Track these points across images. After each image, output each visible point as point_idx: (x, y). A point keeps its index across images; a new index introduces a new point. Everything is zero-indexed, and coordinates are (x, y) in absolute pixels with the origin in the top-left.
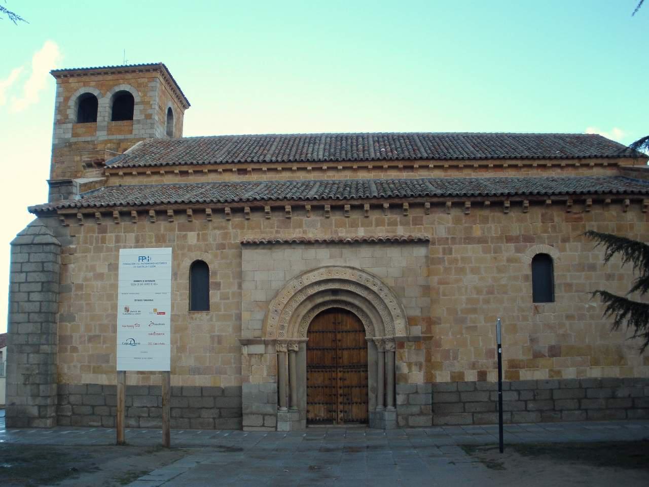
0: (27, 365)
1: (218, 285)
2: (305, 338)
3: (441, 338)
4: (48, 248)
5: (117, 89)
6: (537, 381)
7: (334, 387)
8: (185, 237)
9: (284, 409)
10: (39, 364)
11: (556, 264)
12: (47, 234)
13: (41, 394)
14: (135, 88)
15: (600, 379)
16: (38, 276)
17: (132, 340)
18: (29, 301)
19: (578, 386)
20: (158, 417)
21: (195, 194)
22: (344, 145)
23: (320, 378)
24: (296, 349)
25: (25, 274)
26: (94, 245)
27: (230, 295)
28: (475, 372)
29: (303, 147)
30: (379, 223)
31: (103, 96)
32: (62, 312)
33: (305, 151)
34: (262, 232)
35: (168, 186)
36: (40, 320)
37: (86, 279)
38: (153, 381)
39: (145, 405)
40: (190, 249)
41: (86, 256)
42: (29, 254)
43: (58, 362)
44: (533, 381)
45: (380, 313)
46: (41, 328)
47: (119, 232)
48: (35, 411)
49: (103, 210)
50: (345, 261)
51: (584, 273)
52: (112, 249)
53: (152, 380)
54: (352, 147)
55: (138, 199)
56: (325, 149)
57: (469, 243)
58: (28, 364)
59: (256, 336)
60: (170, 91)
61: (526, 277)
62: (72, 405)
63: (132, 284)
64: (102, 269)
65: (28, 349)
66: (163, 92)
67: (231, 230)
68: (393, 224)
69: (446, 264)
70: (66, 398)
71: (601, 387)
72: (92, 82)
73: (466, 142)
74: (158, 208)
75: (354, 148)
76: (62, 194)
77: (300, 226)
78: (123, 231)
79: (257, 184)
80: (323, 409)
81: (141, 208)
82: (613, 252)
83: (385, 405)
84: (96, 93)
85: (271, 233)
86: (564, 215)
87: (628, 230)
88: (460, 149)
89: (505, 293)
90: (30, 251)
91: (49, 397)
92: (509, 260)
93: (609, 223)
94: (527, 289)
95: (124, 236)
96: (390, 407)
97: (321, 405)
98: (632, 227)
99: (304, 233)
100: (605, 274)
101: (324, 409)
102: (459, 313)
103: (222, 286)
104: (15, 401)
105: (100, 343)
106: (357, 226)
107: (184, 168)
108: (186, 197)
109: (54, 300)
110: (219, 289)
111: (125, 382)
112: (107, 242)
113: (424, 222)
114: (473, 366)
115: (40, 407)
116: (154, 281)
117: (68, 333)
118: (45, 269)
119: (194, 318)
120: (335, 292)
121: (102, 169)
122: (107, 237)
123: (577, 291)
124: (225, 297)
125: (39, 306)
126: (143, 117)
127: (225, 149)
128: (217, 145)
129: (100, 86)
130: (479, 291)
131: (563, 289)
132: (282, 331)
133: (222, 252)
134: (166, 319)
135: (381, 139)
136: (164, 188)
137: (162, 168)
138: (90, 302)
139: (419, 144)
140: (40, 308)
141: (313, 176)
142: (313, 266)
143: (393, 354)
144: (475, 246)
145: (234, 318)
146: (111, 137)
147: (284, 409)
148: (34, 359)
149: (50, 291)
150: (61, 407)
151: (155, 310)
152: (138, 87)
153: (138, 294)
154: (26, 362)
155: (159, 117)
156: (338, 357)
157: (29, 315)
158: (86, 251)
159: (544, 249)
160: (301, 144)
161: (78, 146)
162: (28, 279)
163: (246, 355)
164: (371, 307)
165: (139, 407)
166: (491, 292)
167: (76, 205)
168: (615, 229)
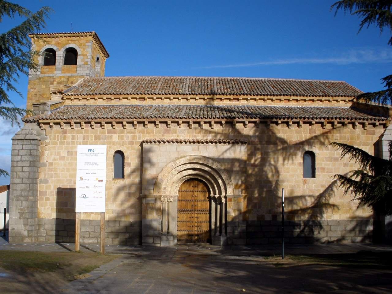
0: (21, 208)
2: (177, 195)
4: (34, 142)
5: (68, 46)
8: (111, 137)
10: (28, 207)
11: (316, 156)
12: (33, 134)
13: (29, 224)
14: (78, 46)
16: (28, 157)
17: (85, 196)
18: (22, 171)
19: (327, 224)
20: (94, 237)
21: (116, 112)
22: (200, 84)
23: (185, 217)
25: (20, 156)
26: (60, 140)
28: (270, 215)
29: (177, 85)
31: (59, 50)
32: (41, 178)
34: (154, 136)
35: (100, 106)
36: (29, 183)
37: (55, 160)
38: (92, 218)
39: (87, 231)
40: (114, 144)
41: (55, 146)
42: (23, 145)
43: (38, 206)
46: (29, 187)
47: (74, 134)
48: (26, 233)
51: (332, 162)
52: (69, 143)
53: (91, 217)
54: (204, 85)
55: (85, 115)
56: (189, 87)
58: (22, 207)
61: (300, 163)
62: (46, 230)
63: (84, 165)
64: (64, 153)
65: (22, 198)
67: (137, 134)
70: (42, 226)
71: (339, 225)
72: (52, 42)
73: (269, 85)
75: (206, 87)
76: (41, 111)
77: (176, 133)
78: (76, 133)
79: (151, 107)
82: (345, 154)
84: (55, 48)
85: (160, 136)
87: (357, 139)
88: (266, 89)
89: (288, 172)
90: (23, 144)
91: (34, 225)
93: (346, 135)
95: (77, 136)
96: (223, 234)
98: (358, 137)
99: (178, 136)
100: (343, 163)
103: (131, 165)
104: (14, 228)
107: (109, 96)
108: (112, 115)
109: (37, 171)
111: (80, 218)
112: (67, 139)
114: (269, 212)
115: (28, 231)
116: (97, 163)
117: (44, 190)
118: (32, 154)
119: (116, 182)
121: (62, 95)
122: (67, 136)
123: (328, 172)
125: (28, 174)
126: (83, 63)
127: (132, 85)
128: (127, 82)
129: (58, 44)
131: (320, 171)
132: (164, 191)
133: (132, 146)
134: (103, 184)
135: (221, 82)
136: (98, 108)
138: (56, 172)
139: (243, 85)
140: (29, 176)
141: (183, 102)
142: (182, 155)
146: (64, 75)
148: (25, 204)
149: (35, 166)
150: (40, 231)
151: (97, 179)
152: (80, 45)
153: (88, 170)
154: (21, 206)
157: (22, 180)
158: (55, 143)
160: (175, 83)
161: (44, 79)
162: (22, 159)
163: (145, 204)
165: (84, 232)
168: (350, 139)
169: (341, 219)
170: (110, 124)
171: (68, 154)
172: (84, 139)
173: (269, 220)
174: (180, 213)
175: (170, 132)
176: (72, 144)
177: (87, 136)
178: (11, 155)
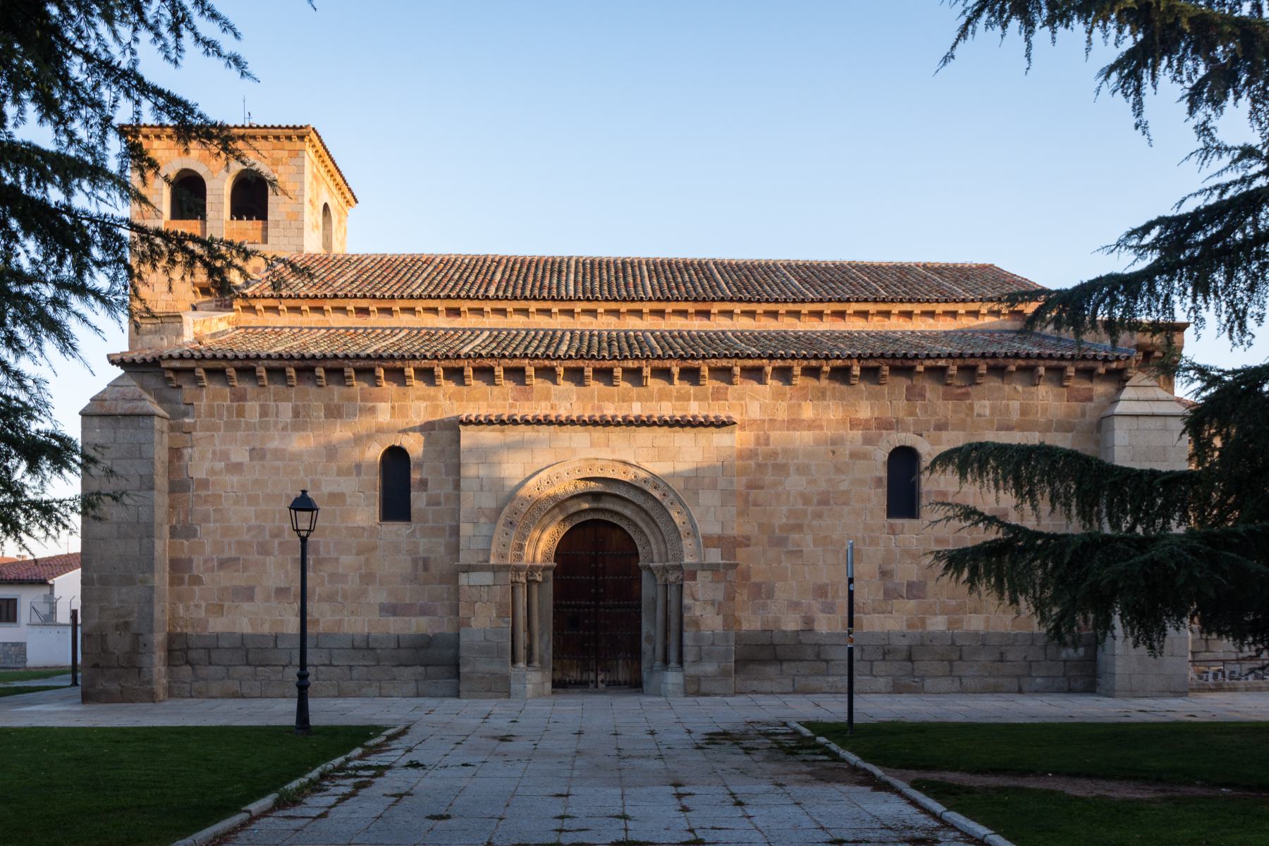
1: (423, 484)
6: (888, 634)
9: (522, 665)
15: (982, 633)
19: (950, 642)
24: (539, 579)
27: (442, 500)
30: (662, 396)
33: (547, 282)
37: (212, 472)
41: (213, 436)
44: (883, 632)
45: (663, 529)
49: (359, 364)
50: (613, 452)
57: (794, 429)
60: (325, 174)
61: (879, 480)
64: (240, 454)
66: (315, 177)
68: (684, 398)
74: (329, 364)
81: (301, 364)
83: (666, 661)
86: (941, 389)
89: (846, 503)
92: (854, 455)
94: (879, 498)
96: (673, 664)
102: (777, 530)
105: (238, 570)
106: (631, 400)
107: (363, 303)
113: (729, 397)
124: (434, 502)
130: (806, 500)
137: (328, 301)
141: (559, 323)
145: (447, 533)
147: (522, 665)
155: (312, 217)
158: (213, 428)
159: (908, 439)
164: (647, 519)
166: (824, 502)
167: (193, 355)
169: (990, 630)
170: (298, 721)
171: (250, 456)
172: (296, 414)
173: (794, 628)
176: (261, 428)
177: (304, 406)
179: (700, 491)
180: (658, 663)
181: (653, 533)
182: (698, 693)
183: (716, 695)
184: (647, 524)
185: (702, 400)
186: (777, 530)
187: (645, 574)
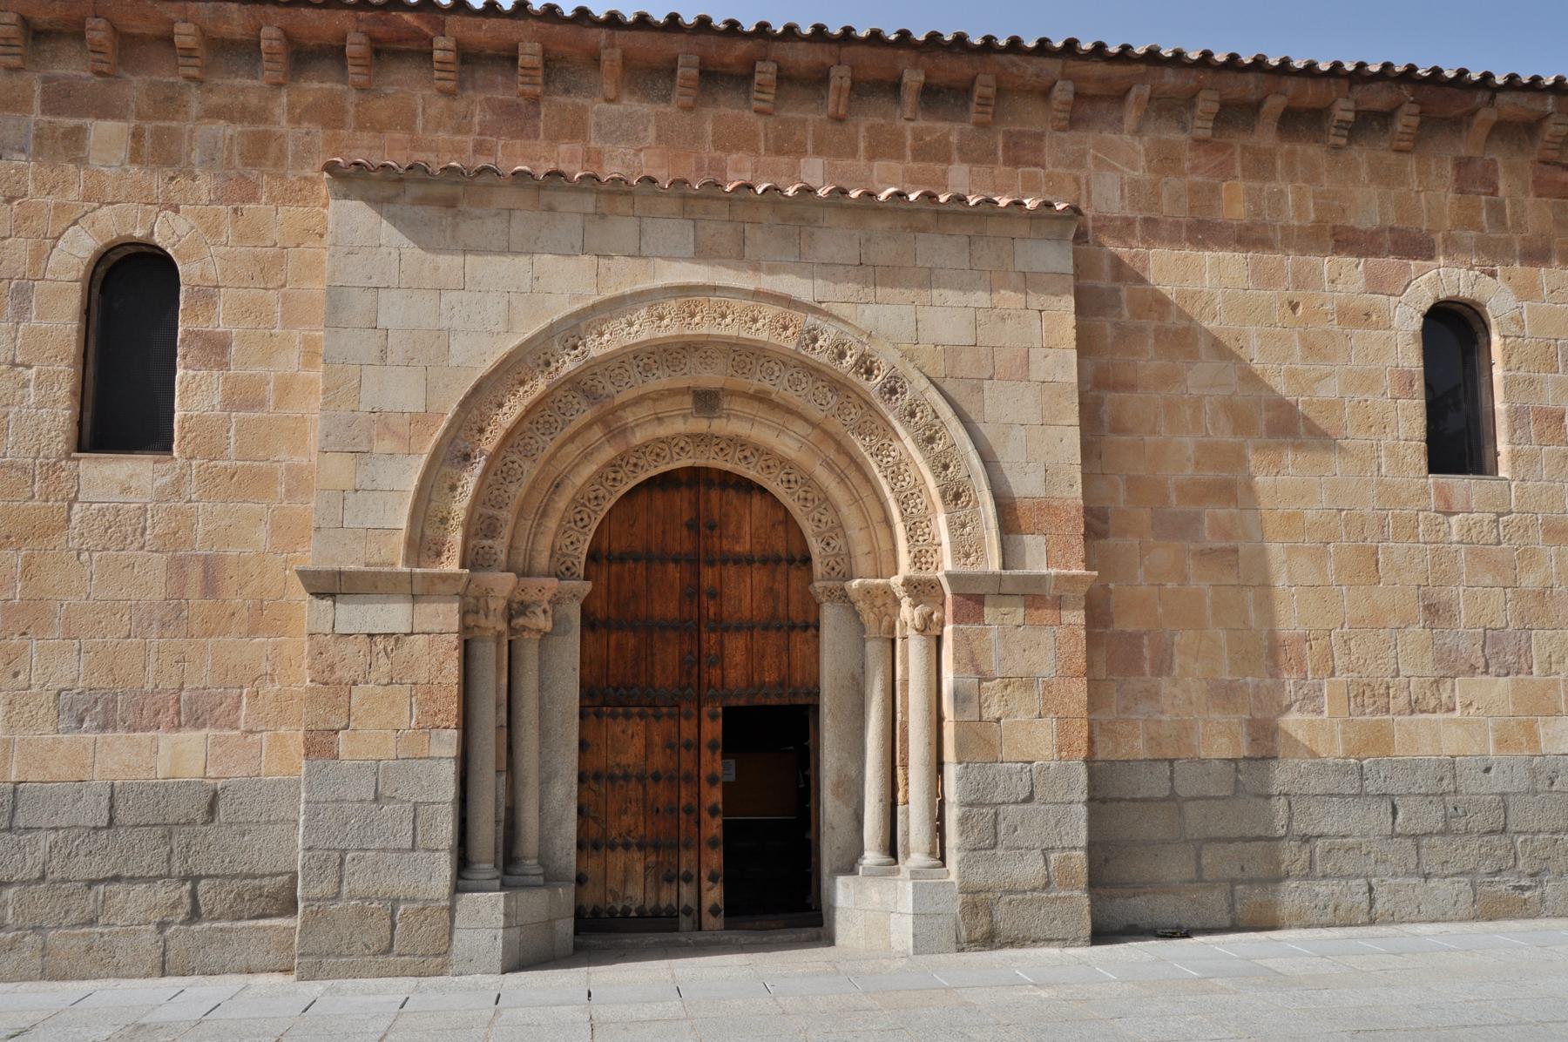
3: (1110, 591)
7: (688, 779)
59: (376, 558)
69: (1126, 313)
80: (639, 867)
97: (636, 855)
101: (646, 868)
102: (1173, 498)
110: (223, 365)
113: (1048, 160)
120: (706, 401)
143: (889, 645)
144: (1226, 255)
156: (703, 660)
174: (598, 715)
175: (536, 128)
178: (167, 980)
179: (987, 384)
180: (872, 856)
181: (857, 500)
182: (990, 940)
183: (1049, 941)
184: (842, 480)
185: (977, 161)
186: (1173, 498)
187: (830, 615)
